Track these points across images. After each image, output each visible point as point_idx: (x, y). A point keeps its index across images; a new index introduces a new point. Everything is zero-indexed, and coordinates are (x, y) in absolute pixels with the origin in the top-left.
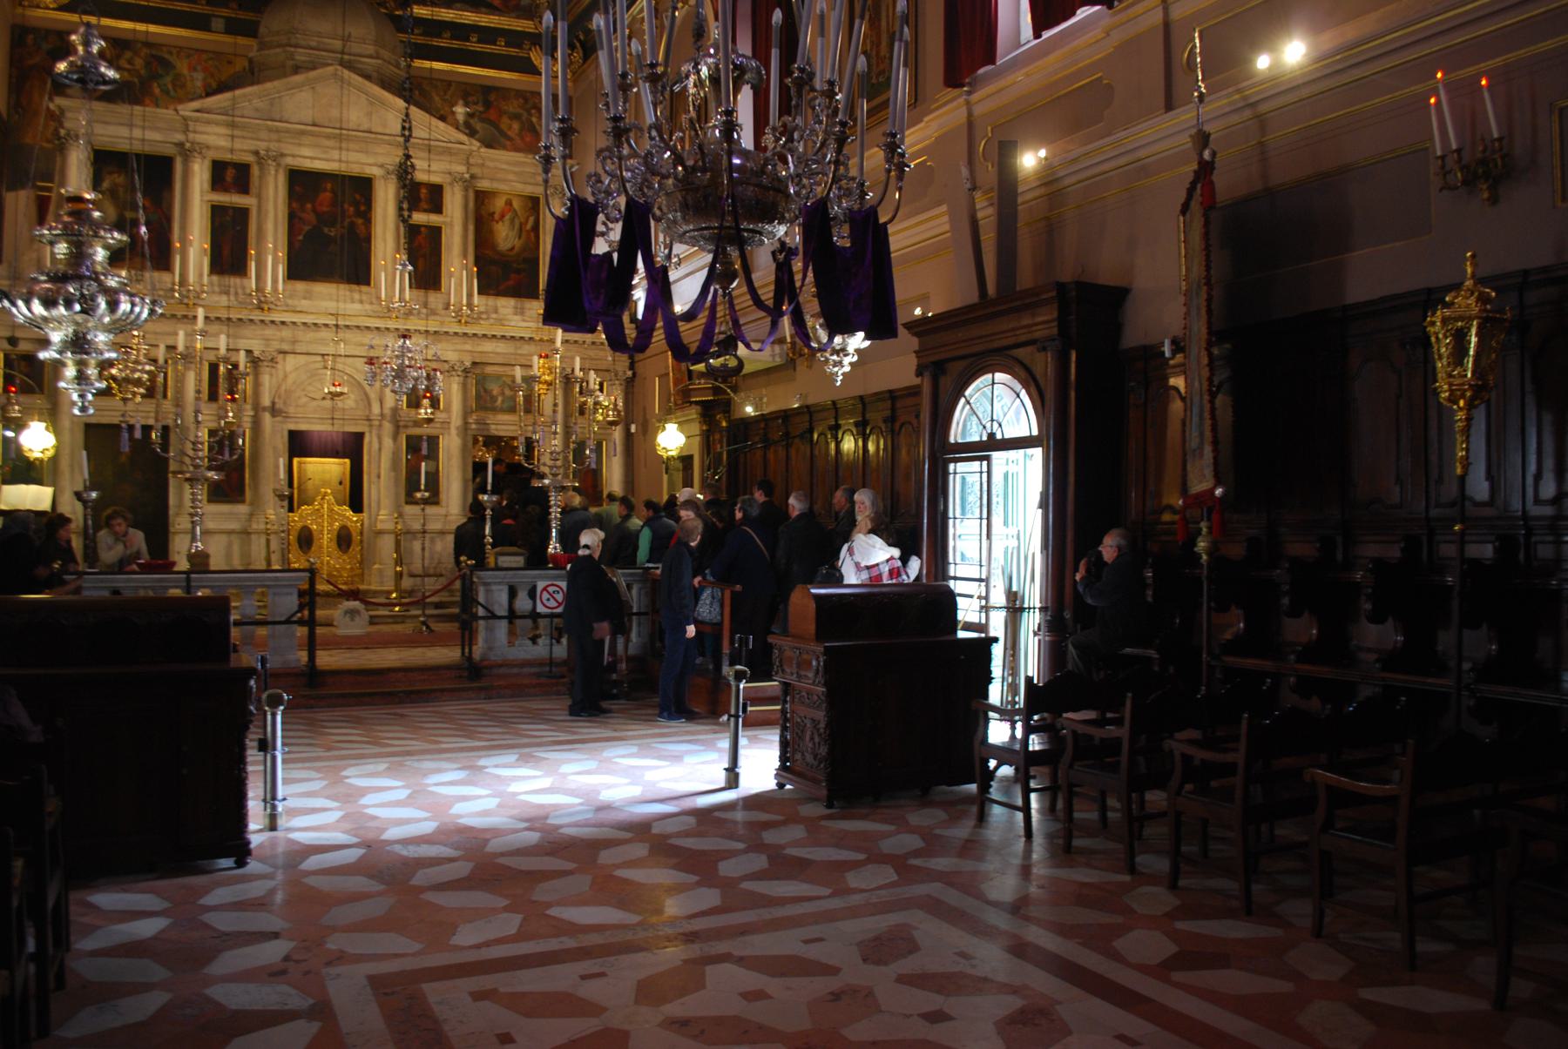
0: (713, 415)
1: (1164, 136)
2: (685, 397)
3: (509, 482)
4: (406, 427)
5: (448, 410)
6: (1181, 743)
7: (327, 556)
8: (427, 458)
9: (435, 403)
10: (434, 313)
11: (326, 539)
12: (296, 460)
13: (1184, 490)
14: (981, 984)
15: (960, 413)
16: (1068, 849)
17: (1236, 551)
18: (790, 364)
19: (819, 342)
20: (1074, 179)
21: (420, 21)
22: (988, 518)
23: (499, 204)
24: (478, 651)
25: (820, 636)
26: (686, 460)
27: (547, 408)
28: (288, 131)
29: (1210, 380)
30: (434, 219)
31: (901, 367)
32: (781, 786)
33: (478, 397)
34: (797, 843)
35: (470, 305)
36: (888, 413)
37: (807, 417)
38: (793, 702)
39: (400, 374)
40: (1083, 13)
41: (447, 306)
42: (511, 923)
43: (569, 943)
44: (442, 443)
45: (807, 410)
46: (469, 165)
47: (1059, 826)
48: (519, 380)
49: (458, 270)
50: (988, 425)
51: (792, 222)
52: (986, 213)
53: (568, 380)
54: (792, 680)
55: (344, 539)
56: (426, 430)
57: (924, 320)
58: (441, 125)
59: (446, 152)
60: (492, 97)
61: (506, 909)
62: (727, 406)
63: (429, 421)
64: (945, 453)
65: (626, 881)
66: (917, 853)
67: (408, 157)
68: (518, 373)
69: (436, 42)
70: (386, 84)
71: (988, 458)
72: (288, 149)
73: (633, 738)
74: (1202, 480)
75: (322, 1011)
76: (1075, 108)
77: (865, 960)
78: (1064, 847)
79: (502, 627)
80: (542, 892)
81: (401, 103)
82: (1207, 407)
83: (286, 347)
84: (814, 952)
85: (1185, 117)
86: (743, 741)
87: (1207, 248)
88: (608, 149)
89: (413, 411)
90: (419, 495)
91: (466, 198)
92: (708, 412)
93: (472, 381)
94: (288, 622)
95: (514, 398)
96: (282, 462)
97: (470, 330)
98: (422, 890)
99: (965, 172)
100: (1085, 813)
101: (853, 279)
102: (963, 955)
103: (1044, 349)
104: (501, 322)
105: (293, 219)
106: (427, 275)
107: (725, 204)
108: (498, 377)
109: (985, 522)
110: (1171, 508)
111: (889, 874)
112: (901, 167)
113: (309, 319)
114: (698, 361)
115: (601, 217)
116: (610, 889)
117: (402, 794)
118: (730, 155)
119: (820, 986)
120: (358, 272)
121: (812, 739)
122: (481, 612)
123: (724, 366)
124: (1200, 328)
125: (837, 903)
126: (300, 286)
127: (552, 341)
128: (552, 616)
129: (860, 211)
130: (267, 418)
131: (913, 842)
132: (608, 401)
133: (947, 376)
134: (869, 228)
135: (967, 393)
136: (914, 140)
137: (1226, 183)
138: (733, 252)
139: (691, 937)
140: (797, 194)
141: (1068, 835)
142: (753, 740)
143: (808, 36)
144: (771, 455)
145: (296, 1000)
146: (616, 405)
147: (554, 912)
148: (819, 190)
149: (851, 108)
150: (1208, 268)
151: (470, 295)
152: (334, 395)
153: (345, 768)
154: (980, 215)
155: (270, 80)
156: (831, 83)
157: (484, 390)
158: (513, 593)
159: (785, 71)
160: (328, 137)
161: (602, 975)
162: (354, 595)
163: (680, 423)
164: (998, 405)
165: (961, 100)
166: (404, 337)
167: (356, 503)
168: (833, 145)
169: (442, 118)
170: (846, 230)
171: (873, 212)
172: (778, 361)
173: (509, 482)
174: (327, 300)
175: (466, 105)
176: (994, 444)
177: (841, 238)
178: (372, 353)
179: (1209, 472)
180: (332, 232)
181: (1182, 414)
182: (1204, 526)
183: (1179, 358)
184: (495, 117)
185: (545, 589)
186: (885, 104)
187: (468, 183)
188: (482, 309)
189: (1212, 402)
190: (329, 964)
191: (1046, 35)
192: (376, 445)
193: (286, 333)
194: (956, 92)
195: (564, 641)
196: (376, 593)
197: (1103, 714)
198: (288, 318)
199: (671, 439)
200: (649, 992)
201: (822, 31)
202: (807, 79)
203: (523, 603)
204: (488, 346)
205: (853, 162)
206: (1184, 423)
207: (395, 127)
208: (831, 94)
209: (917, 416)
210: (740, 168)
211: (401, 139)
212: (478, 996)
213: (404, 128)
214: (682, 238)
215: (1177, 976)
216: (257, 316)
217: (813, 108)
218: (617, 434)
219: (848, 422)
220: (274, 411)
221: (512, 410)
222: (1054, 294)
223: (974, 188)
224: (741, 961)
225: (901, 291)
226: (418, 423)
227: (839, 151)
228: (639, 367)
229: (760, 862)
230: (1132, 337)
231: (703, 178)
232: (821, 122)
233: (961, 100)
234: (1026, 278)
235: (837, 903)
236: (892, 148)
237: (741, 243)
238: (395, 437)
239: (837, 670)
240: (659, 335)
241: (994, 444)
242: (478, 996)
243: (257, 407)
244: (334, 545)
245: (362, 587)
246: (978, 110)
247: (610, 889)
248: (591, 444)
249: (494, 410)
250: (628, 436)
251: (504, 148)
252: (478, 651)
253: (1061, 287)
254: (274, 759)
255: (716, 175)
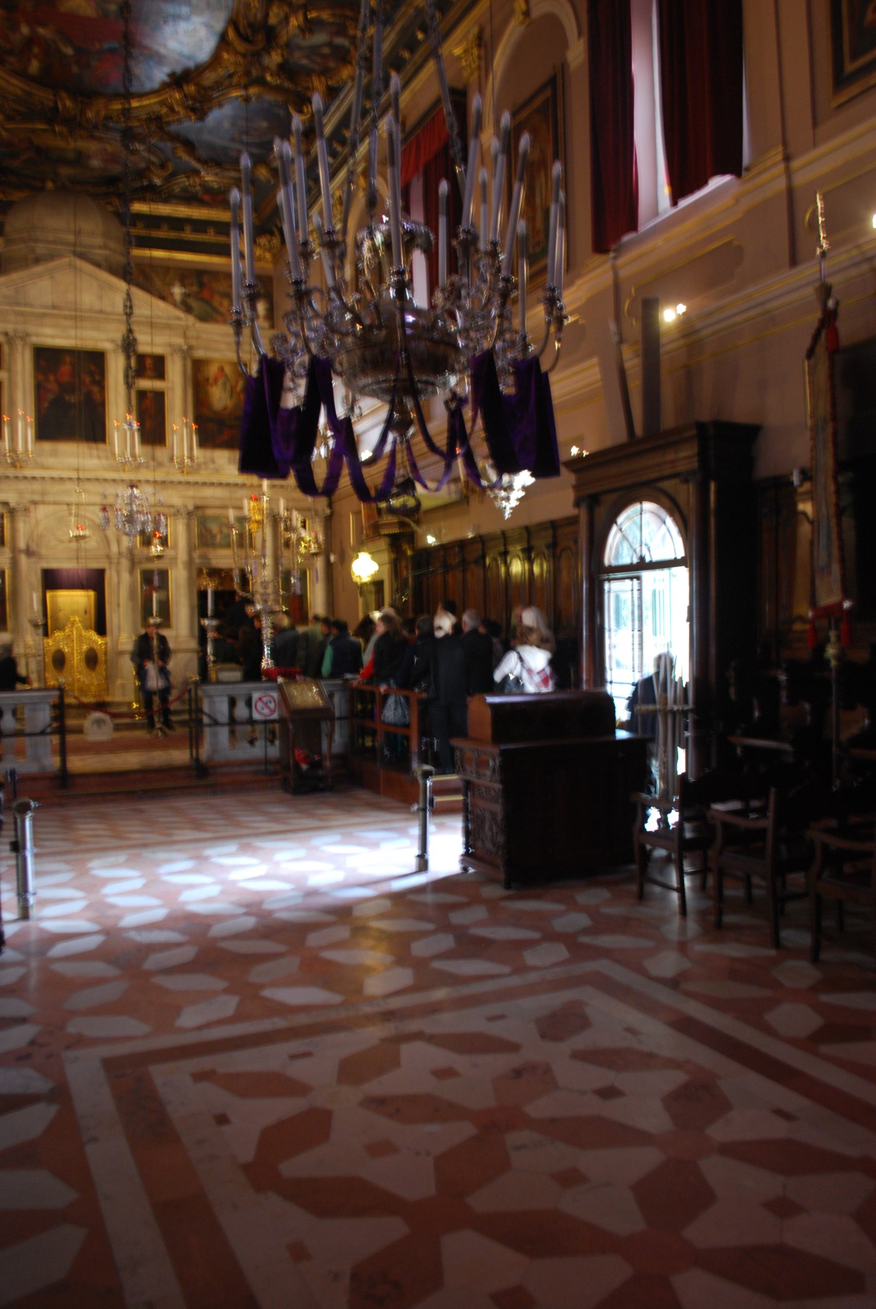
0: (400, 543)
1: (789, 290)
2: (375, 530)
3: (226, 605)
4: (140, 563)
5: (175, 547)
6: (818, 834)
7: (77, 674)
8: (158, 589)
9: (164, 542)
10: (160, 465)
11: (76, 660)
12: (49, 594)
13: (813, 604)
14: (647, 1060)
15: (614, 538)
16: (719, 925)
17: (861, 656)
18: (464, 500)
19: (488, 480)
20: (709, 331)
21: (140, 216)
22: (640, 630)
23: (213, 370)
24: (205, 752)
25: (497, 738)
26: (377, 584)
27: (258, 542)
28: (32, 314)
29: (837, 505)
30: (157, 385)
31: (561, 500)
32: (465, 869)
33: (201, 536)
34: (480, 924)
35: (191, 457)
36: (550, 540)
37: (480, 546)
38: (473, 796)
39: (130, 519)
40: (717, 182)
41: (171, 459)
42: (229, 1005)
43: (279, 1023)
44: (172, 575)
45: (481, 540)
46: (185, 336)
47: (710, 903)
48: (232, 519)
49: (180, 427)
50: (638, 550)
51: (461, 372)
52: (633, 363)
53: (275, 519)
54: (473, 778)
55: (92, 659)
56: (156, 565)
57: (579, 457)
58: (161, 304)
59: (164, 326)
60: (205, 279)
61: (227, 991)
62: (411, 537)
63: (159, 557)
64: (599, 573)
65: (330, 963)
66: (586, 931)
67: (130, 331)
68: (232, 514)
69: (155, 234)
70: (113, 270)
71: (638, 578)
72: (32, 329)
73: (338, 826)
74: (831, 594)
75: (60, 1094)
76: (712, 266)
77: (543, 1036)
78: (715, 926)
79: (224, 733)
80: (257, 974)
81: (123, 285)
82: (834, 530)
83: (37, 498)
84: (496, 1029)
85: (808, 272)
86: (431, 828)
87: (833, 389)
88: (293, 312)
89: (145, 550)
90: (152, 621)
91: (185, 366)
92: (396, 543)
93: (195, 523)
94: (43, 733)
95: (229, 536)
96: (36, 597)
97: (192, 478)
98: (151, 973)
99: (613, 327)
100: (733, 891)
101: (519, 425)
102: (630, 1030)
103: (686, 481)
104: (217, 471)
105: (40, 390)
106: (153, 431)
107: (401, 361)
108: (216, 518)
109: (636, 633)
110: (802, 619)
111: (560, 952)
112: (560, 320)
113: (55, 474)
114: (381, 499)
115: (289, 374)
116: (318, 971)
117: (138, 883)
118: (403, 311)
119: (504, 1062)
120: (94, 431)
121: (491, 829)
122: (206, 720)
123: (404, 506)
124: (827, 460)
125: (515, 981)
126: (47, 446)
127: (260, 486)
128: (266, 722)
129: (523, 361)
130: (23, 559)
131: (582, 920)
132: (309, 538)
133: (601, 507)
134: (533, 377)
135: (621, 519)
136: (571, 298)
137: (849, 330)
138: (409, 403)
139: (388, 1016)
140: (466, 346)
141: (720, 913)
142: (440, 826)
143: (471, 208)
144: (450, 579)
145: (39, 1084)
146: (316, 538)
147: (267, 993)
148: (486, 345)
149: (513, 269)
150: (834, 405)
151: (191, 449)
152: (78, 538)
153: (90, 860)
154: (627, 365)
155: (15, 270)
156: (494, 244)
157: (205, 528)
158: (232, 702)
159: (452, 233)
160: (66, 318)
161: (307, 1055)
162: (101, 706)
163: (372, 553)
164: (647, 531)
165: (608, 265)
166: (132, 487)
167: (101, 628)
168: (497, 301)
169: (163, 298)
170: (510, 380)
171: (535, 362)
172: (454, 497)
173: (226, 605)
174: (70, 456)
175: (183, 285)
176: (643, 565)
177: (507, 387)
178: (104, 502)
179: (837, 587)
180: (72, 399)
181: (809, 536)
182: (832, 634)
183: (807, 486)
184: (203, 294)
185: (260, 699)
186: (544, 270)
187: (186, 353)
188: (201, 460)
189: (839, 525)
190: (69, 1047)
191: (684, 203)
192: (115, 579)
193: (37, 486)
194: (603, 258)
195: (277, 742)
196: (119, 704)
197: (747, 804)
198: (38, 473)
199: (365, 567)
200: (352, 1070)
201: (485, 199)
202: (472, 240)
203: (241, 711)
204: (208, 492)
205: (516, 323)
206: (812, 543)
207: (120, 308)
208: (494, 254)
209: (576, 542)
210: (413, 325)
211: (124, 317)
212: (199, 1077)
213: (126, 306)
214: (364, 391)
215: (825, 1049)
216: (11, 472)
217: (479, 268)
218: (319, 563)
219: (516, 549)
220: (29, 552)
221: (228, 546)
222: (694, 432)
223: (621, 341)
224: (431, 1039)
225: (562, 432)
226: (150, 559)
227: (503, 305)
228: (337, 506)
229: (447, 941)
230: (765, 469)
231: (380, 335)
232: (485, 281)
233: (608, 265)
234: (669, 419)
235: (515, 981)
236: (552, 302)
237: (415, 394)
238: (132, 571)
239: (512, 770)
240: (345, 481)
241: (643, 565)
242: (199, 1077)
243: (14, 550)
244: (83, 664)
245: (109, 699)
246: (623, 273)
247: (318, 971)
248: (296, 573)
249: (214, 545)
250: (328, 565)
251: (216, 321)
252: (205, 752)
253: (701, 427)
254: (25, 859)
255: (392, 331)
